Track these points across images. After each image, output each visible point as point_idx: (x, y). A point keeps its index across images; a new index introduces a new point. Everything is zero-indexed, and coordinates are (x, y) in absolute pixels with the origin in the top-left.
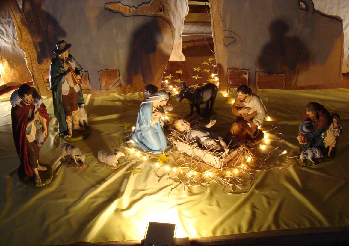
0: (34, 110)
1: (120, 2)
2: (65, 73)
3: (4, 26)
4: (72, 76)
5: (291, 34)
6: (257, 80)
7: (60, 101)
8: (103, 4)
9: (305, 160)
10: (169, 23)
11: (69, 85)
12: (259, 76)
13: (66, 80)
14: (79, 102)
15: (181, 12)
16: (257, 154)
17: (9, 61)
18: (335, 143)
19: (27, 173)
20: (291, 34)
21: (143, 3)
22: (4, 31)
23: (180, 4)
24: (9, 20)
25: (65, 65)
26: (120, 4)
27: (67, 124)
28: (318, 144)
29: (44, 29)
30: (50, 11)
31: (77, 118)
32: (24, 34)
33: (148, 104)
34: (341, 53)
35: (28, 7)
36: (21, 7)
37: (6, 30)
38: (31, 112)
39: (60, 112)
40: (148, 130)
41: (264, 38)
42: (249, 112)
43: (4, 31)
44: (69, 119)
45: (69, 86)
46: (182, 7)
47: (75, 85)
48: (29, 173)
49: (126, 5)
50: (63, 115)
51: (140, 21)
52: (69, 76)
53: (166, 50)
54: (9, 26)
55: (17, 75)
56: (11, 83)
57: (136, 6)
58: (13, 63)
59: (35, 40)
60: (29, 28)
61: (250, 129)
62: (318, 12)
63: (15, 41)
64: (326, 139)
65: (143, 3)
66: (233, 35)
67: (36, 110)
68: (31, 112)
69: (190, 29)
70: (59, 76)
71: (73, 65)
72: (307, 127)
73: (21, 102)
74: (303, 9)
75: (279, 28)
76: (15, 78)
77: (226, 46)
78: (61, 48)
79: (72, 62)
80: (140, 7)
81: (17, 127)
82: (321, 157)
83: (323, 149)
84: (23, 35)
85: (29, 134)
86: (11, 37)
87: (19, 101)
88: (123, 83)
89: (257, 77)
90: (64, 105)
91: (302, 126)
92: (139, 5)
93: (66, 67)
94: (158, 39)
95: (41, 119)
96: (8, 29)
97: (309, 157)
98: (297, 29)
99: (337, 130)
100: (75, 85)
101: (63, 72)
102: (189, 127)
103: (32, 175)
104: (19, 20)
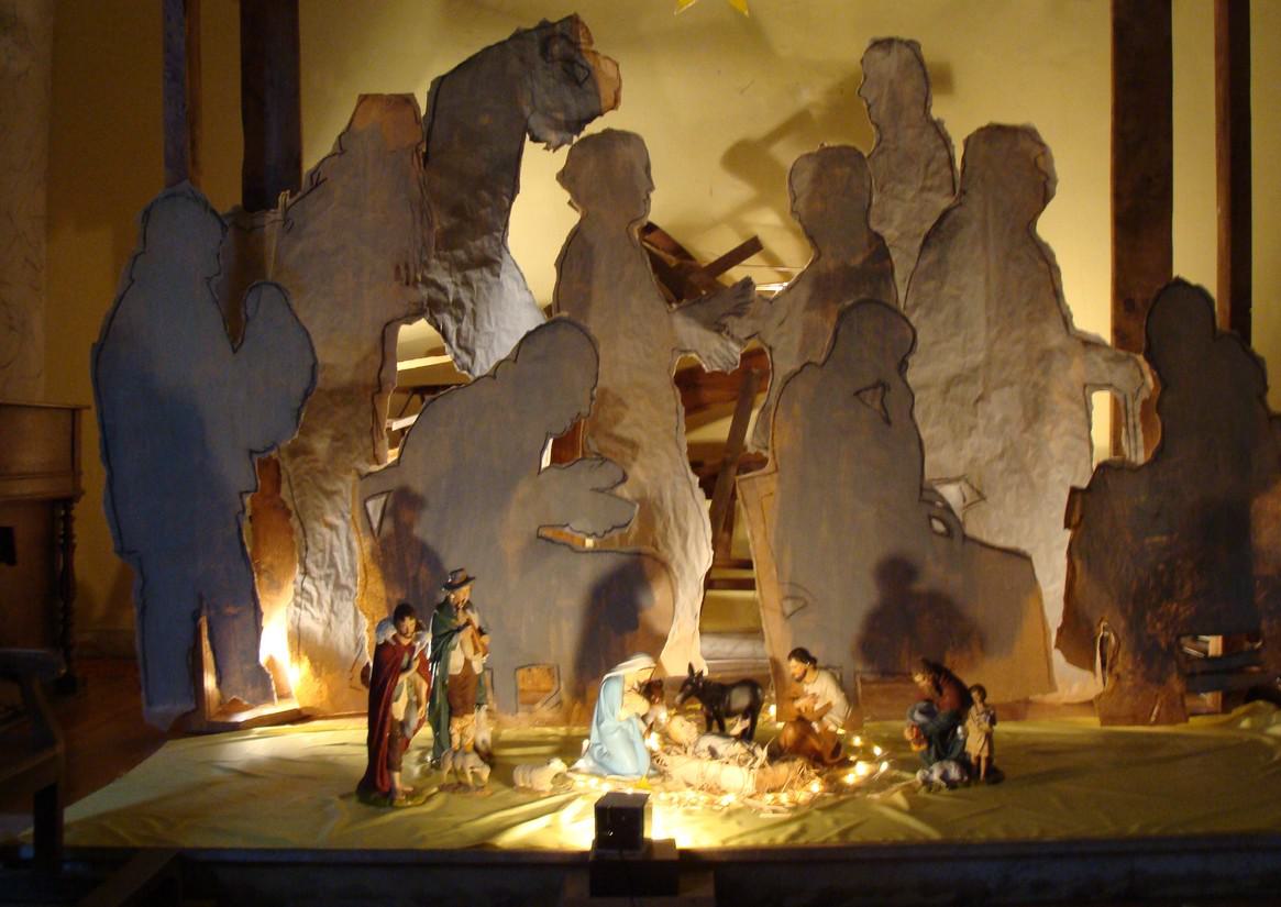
0: (413, 654)
1: (567, 525)
2: (459, 630)
3: (317, 583)
4: (472, 637)
5: (921, 586)
6: (860, 690)
7: (443, 682)
8: (535, 527)
9: (927, 782)
10: (664, 566)
11: (464, 652)
12: (863, 681)
13: (458, 645)
14: (478, 701)
15: (696, 563)
16: (835, 786)
17: (312, 661)
18: (986, 747)
19: (379, 784)
20: (921, 586)
21: (614, 527)
22: (314, 594)
23: (694, 546)
24: (328, 572)
25: (460, 613)
26: (567, 530)
27: (450, 736)
28: (955, 754)
29: (411, 574)
30: (429, 538)
31: (471, 732)
32: (371, 580)
33: (616, 677)
34: (1044, 629)
35: (388, 526)
36: (375, 525)
37: (319, 594)
38: (406, 660)
39: (440, 709)
40: (615, 731)
41: (867, 596)
42: (815, 703)
43: (314, 594)
44: (457, 724)
45: (463, 657)
46: (699, 552)
47: (475, 654)
48: (383, 784)
49: (580, 532)
50: (444, 718)
51: (606, 563)
52: (466, 635)
53: (659, 626)
54: (327, 585)
55: (325, 694)
56: (311, 708)
57: (600, 534)
58: (321, 666)
59: (391, 595)
60: (383, 567)
61: (818, 737)
62: (974, 540)
63: (333, 618)
64: (969, 741)
65: (614, 527)
66: (801, 593)
67: (416, 655)
68: (406, 660)
69: (735, 647)
70: (446, 634)
71: (475, 618)
72: (922, 712)
73: (394, 637)
74: (941, 534)
75: (896, 573)
76: (319, 701)
77: (787, 617)
78: (457, 582)
79: (473, 612)
80: (607, 536)
81: (381, 681)
82: (962, 778)
83: (964, 763)
84: (369, 582)
85: (397, 700)
86: (326, 607)
87: (391, 632)
88: (566, 697)
89: (859, 685)
90: (449, 698)
91: (913, 712)
92: (605, 532)
93: (462, 620)
94: (644, 600)
95: (418, 683)
96: (323, 591)
97: (936, 777)
98: (934, 575)
99: (983, 716)
100: (475, 654)
101: (455, 628)
102: (695, 729)
103: (386, 789)
104: (367, 550)
